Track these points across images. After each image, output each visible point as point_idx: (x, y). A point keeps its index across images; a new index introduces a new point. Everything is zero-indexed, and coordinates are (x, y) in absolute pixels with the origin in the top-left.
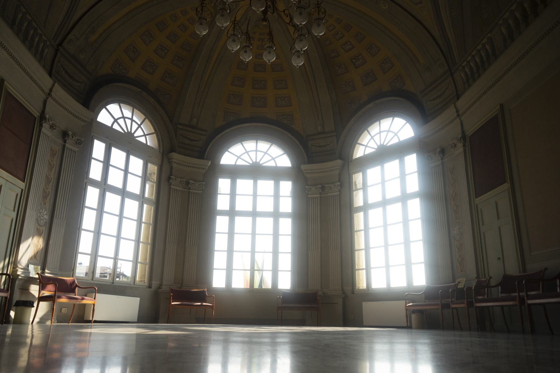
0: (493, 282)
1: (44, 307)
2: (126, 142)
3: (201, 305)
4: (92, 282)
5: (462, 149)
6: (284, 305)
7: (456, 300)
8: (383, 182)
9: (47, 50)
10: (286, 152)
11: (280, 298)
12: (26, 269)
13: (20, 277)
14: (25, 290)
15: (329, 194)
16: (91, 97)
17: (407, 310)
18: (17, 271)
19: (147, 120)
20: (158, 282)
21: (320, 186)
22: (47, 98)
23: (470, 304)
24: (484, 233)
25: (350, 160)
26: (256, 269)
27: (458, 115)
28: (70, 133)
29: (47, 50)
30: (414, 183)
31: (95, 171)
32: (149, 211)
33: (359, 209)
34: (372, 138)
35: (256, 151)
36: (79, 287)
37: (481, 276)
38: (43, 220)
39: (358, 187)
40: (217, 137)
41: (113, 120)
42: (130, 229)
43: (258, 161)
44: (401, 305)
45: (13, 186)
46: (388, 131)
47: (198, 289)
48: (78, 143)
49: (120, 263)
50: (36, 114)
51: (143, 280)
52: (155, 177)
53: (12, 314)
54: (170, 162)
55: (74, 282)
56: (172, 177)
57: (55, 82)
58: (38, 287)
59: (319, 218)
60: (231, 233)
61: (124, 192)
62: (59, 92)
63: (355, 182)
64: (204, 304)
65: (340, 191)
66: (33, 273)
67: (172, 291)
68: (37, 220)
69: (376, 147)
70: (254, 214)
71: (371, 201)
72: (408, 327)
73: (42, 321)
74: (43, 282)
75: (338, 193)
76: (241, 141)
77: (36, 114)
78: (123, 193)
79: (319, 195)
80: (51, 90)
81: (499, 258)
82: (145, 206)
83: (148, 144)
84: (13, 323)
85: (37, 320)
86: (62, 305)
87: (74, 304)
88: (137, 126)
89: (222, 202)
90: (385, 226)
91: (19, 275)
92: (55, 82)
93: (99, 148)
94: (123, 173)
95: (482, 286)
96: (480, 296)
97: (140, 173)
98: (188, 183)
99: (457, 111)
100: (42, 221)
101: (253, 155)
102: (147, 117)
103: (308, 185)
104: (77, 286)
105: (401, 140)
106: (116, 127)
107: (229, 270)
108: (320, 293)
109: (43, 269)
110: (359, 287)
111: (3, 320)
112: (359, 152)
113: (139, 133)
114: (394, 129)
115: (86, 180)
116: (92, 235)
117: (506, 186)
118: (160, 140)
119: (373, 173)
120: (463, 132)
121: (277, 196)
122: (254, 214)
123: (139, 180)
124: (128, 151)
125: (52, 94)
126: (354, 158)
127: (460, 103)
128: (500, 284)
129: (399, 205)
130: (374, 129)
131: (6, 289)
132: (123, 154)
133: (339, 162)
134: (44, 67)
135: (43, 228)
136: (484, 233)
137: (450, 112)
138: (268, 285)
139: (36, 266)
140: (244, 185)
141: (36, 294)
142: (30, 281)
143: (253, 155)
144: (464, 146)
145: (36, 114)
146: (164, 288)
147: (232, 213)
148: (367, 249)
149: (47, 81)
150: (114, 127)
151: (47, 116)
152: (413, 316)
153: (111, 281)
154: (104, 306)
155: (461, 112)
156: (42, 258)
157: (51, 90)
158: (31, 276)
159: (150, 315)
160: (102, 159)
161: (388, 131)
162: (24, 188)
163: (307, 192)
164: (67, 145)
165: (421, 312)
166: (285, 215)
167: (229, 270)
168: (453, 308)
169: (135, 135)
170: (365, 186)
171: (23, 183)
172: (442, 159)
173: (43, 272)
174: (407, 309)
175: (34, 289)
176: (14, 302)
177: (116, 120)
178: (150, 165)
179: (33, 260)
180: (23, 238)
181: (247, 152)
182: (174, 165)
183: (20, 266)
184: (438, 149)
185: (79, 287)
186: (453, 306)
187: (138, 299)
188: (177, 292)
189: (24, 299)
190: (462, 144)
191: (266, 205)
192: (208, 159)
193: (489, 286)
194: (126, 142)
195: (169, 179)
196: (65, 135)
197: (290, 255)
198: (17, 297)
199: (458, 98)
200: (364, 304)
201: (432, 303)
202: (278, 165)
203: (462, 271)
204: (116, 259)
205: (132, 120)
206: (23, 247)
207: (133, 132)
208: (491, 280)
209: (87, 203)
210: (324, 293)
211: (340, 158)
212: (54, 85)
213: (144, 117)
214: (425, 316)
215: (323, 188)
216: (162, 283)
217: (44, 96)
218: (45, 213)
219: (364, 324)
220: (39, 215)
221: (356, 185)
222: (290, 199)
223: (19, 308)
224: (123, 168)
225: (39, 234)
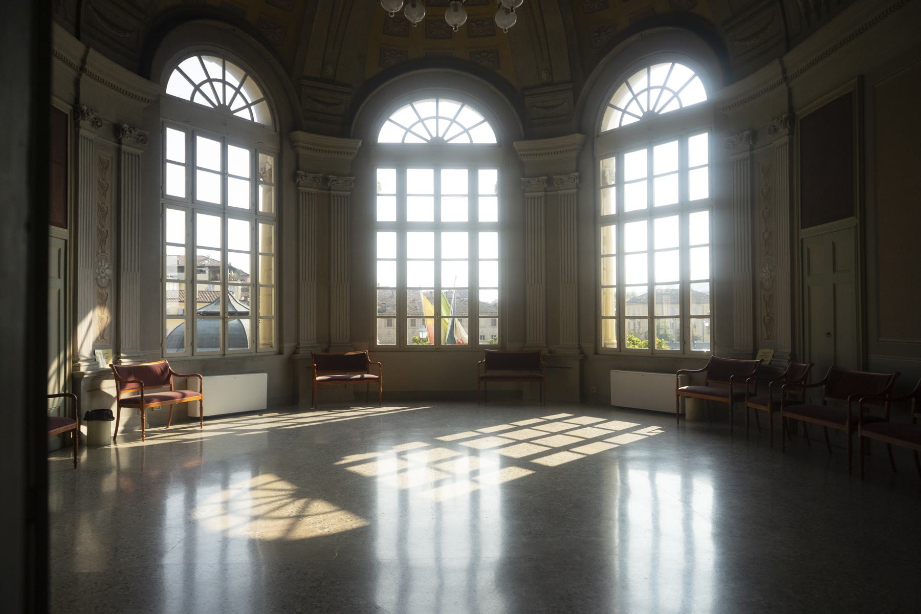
2: (216, 122)
3: (362, 379)
4: (193, 358)
5: (786, 139)
8: (650, 177)
10: (488, 118)
12: (93, 360)
14: (95, 389)
15: (560, 192)
16: (153, 64)
17: (678, 396)
19: (249, 78)
20: (293, 344)
22: (80, 75)
24: (809, 288)
27: (785, 78)
28: (126, 126)
30: (701, 186)
32: (266, 192)
33: (609, 220)
34: (635, 97)
35: (437, 117)
41: (192, 88)
43: (440, 135)
46: (663, 88)
48: (142, 140)
49: (231, 256)
51: (267, 342)
56: (299, 172)
61: (224, 209)
62: (98, 61)
63: (604, 173)
64: (366, 376)
65: (577, 187)
66: (105, 364)
67: (316, 357)
68: (96, 279)
70: (437, 227)
71: (629, 208)
72: (679, 416)
74: (122, 376)
76: (411, 100)
78: (224, 211)
80: (83, 61)
81: (829, 333)
82: (260, 225)
83: (256, 120)
85: (121, 428)
88: (233, 91)
89: (384, 209)
90: (651, 251)
91: (83, 374)
92: (88, 47)
94: (219, 177)
97: (247, 173)
98: (326, 180)
99: (784, 71)
100: (104, 281)
101: (431, 124)
103: (524, 176)
104: (171, 373)
105: (684, 105)
106: (199, 99)
110: (605, 344)
112: (612, 121)
114: (672, 84)
117: (853, 221)
118: (275, 109)
119: (635, 161)
120: (791, 109)
121: (473, 195)
123: (247, 185)
124: (224, 138)
125: (87, 67)
126: (603, 130)
129: (675, 219)
130: (639, 81)
132: (216, 146)
133: (578, 137)
135: (107, 291)
137: (770, 72)
139: (105, 351)
140: (419, 178)
141: (113, 392)
142: (102, 375)
143: (431, 124)
144: (791, 133)
146: (301, 351)
147: (401, 227)
148: (620, 254)
150: (195, 100)
151: (85, 108)
152: (689, 404)
153: (222, 353)
156: (113, 339)
157: (83, 61)
158: (101, 366)
159: (284, 399)
161: (663, 88)
162: (67, 238)
164: (124, 147)
166: (488, 227)
169: (233, 108)
170: (620, 183)
171: (65, 230)
172: (752, 149)
173: (117, 360)
174: (679, 393)
175: (109, 386)
176: (84, 412)
177: (197, 88)
178: (261, 156)
180: (79, 315)
181: (421, 120)
182: (302, 152)
183: (82, 358)
184: (747, 132)
189: (96, 406)
190: (787, 131)
191: (455, 210)
194: (216, 122)
196: (117, 131)
197: (496, 263)
198: (87, 405)
199: (788, 49)
202: (474, 142)
204: (224, 250)
205: (224, 82)
206: (82, 329)
209: (169, 238)
210: (550, 352)
211: (580, 131)
212: (87, 52)
215: (550, 181)
216: (298, 344)
217: (74, 73)
219: (614, 402)
221: (604, 178)
222: (496, 198)
223: (94, 423)
225: (102, 304)
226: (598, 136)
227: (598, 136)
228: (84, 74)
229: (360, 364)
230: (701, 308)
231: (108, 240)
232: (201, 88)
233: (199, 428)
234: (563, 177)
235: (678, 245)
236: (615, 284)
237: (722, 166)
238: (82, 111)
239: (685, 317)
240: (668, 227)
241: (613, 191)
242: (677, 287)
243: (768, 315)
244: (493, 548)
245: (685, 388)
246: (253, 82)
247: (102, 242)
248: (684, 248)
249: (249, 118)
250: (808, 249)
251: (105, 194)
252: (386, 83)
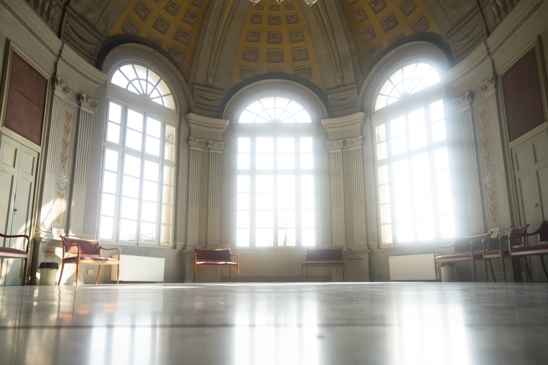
0: (529, 230)
1: (70, 269)
2: (142, 103)
4: (117, 244)
5: (493, 91)
6: (308, 262)
7: (490, 250)
9: (54, 10)
11: (304, 255)
13: (43, 240)
14: (50, 252)
17: (436, 263)
18: (40, 234)
19: (162, 81)
20: (183, 243)
21: (342, 141)
22: (58, 60)
23: (506, 254)
24: (519, 179)
25: (372, 113)
26: (279, 226)
27: (489, 54)
28: (84, 95)
29: (54, 10)
31: (112, 133)
33: (382, 162)
36: (103, 249)
37: (516, 225)
38: (63, 183)
39: (381, 140)
40: (235, 95)
41: (128, 82)
42: (151, 191)
44: (429, 259)
45: (29, 150)
48: (93, 105)
50: (48, 77)
52: (174, 139)
53: (38, 275)
54: (188, 123)
55: (98, 244)
57: (64, 43)
58: (62, 249)
59: (342, 175)
60: (253, 192)
61: (143, 154)
62: (69, 53)
63: (378, 135)
64: (228, 263)
66: (56, 237)
67: (196, 250)
69: (399, 96)
70: (275, 172)
72: (438, 280)
73: (68, 283)
74: (67, 244)
75: (361, 147)
77: (48, 77)
78: (142, 155)
79: (340, 150)
80: (60, 51)
81: (537, 205)
84: (40, 285)
86: (88, 267)
87: (100, 266)
88: (153, 87)
91: (42, 238)
92: (64, 43)
93: (114, 110)
95: (518, 235)
96: (516, 245)
98: (207, 144)
99: (488, 49)
102: (162, 78)
103: (329, 141)
104: (101, 248)
106: (131, 89)
107: (253, 229)
108: (345, 249)
109: (67, 232)
111: (24, 282)
112: (380, 103)
113: (155, 94)
115: (103, 144)
116: (113, 197)
118: (177, 101)
120: (495, 72)
121: (297, 153)
122: (275, 172)
125: (62, 55)
127: (490, 40)
128: (538, 232)
131: (25, 251)
132: (140, 116)
133: (361, 115)
134: (52, 28)
135: (64, 192)
136: (519, 179)
137: (480, 51)
138: (292, 243)
139: (59, 230)
140: (264, 142)
142: (53, 243)
144: (496, 86)
145: (48, 76)
146: (188, 248)
149: (56, 43)
151: (59, 79)
152: (443, 269)
154: (129, 267)
155: (491, 50)
156: (66, 221)
157: (60, 51)
160: (119, 122)
162: (40, 151)
163: (328, 147)
164: (82, 108)
165: (450, 264)
167: (253, 229)
168: (486, 259)
175: (59, 251)
177: (130, 82)
179: (56, 223)
182: (193, 126)
184: (467, 93)
185: (103, 249)
186: (487, 257)
187: (163, 260)
189: (49, 261)
190: (493, 86)
192: (226, 118)
193: (525, 234)
194: (142, 103)
195: (188, 140)
196: (79, 97)
198: (42, 259)
199: (489, 34)
200: (391, 258)
201: (463, 254)
203: (494, 221)
207: (145, 92)
208: (528, 227)
210: (349, 249)
211: (362, 110)
212: (63, 46)
213: (159, 78)
214: (459, 268)
215: (345, 143)
216: (186, 243)
218: (65, 177)
220: (58, 178)
221: (379, 138)
223: (45, 270)
224: (141, 130)
225: (60, 196)
228: (60, 60)
231: (67, 161)
232: (133, 82)
234: (353, 139)
238: (57, 80)
243: (492, 205)
246: (165, 84)
247: (64, 161)
249: (161, 104)
250: (516, 154)
251: (68, 133)
252: (244, 88)
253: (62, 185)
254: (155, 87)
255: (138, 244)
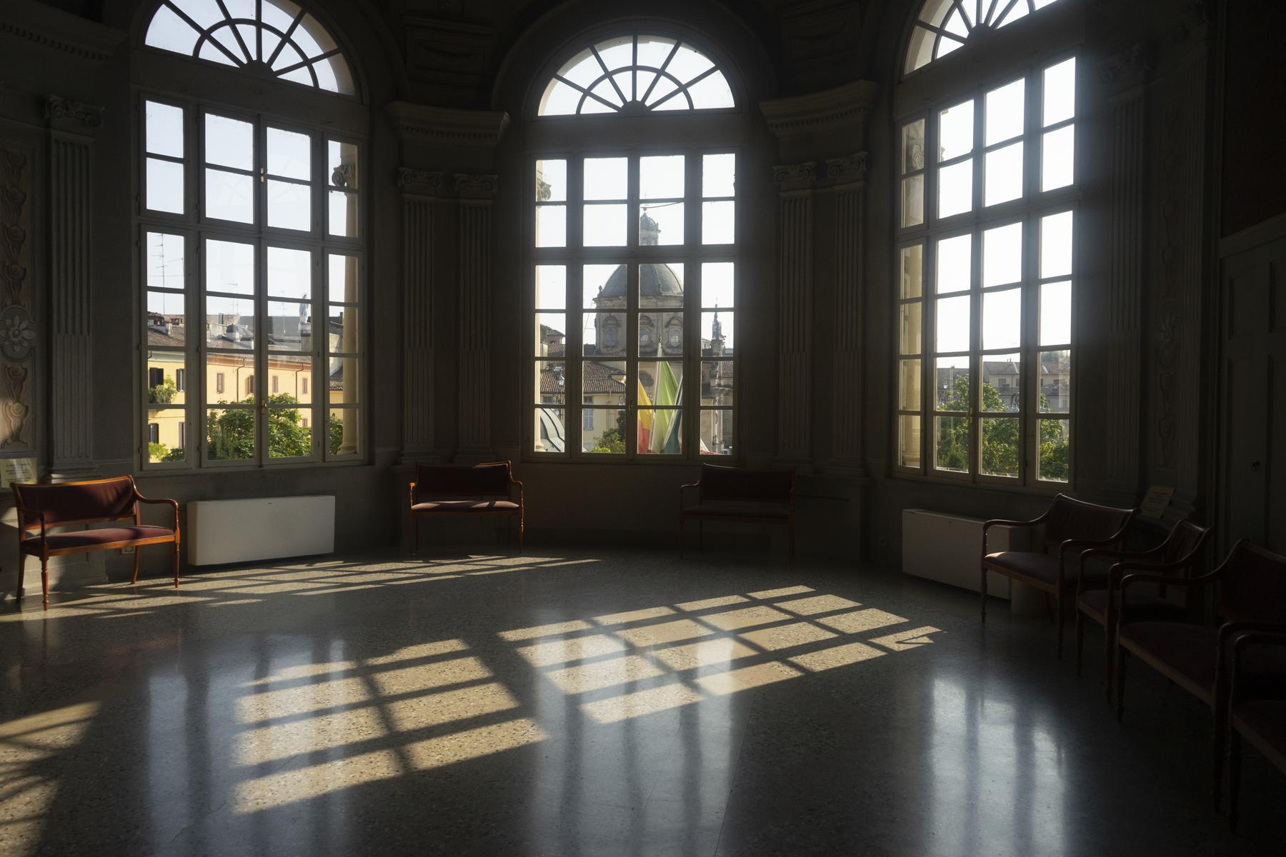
3: (490, 508)
4: (202, 471)
17: (984, 570)
31: (164, 189)
47: (497, 460)
61: (260, 232)
64: (498, 503)
78: (260, 235)
81: (1257, 464)
88: (253, 29)
93: (163, 125)
100: (17, 349)
101: (624, 80)
106: (209, 53)
121: (693, 200)
126: (907, 71)
132: (245, 130)
140: (604, 174)
150: (202, 55)
177: (206, 35)
187: (330, 501)
188: (448, 464)
205: (259, 24)
207: (265, 59)
218: (23, 326)
221: (909, 159)
226: (900, 82)
227: (900, 82)
229: (497, 483)
230: (1056, 399)
233: (172, 588)
235: (1018, 279)
236: (919, 351)
237: (1093, 120)
239: (1028, 415)
240: (1004, 243)
241: (919, 184)
242: (1016, 358)
244: (715, 793)
245: (996, 555)
248: (1031, 284)
249: (310, 83)
253: (17, 349)
254: (286, 38)
255: (261, 466)
